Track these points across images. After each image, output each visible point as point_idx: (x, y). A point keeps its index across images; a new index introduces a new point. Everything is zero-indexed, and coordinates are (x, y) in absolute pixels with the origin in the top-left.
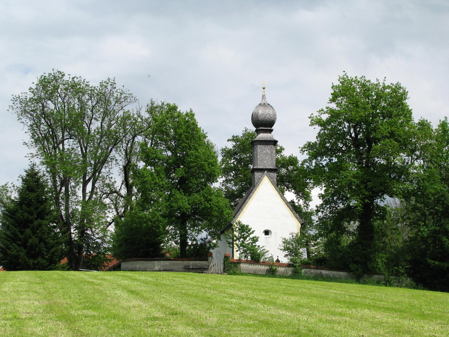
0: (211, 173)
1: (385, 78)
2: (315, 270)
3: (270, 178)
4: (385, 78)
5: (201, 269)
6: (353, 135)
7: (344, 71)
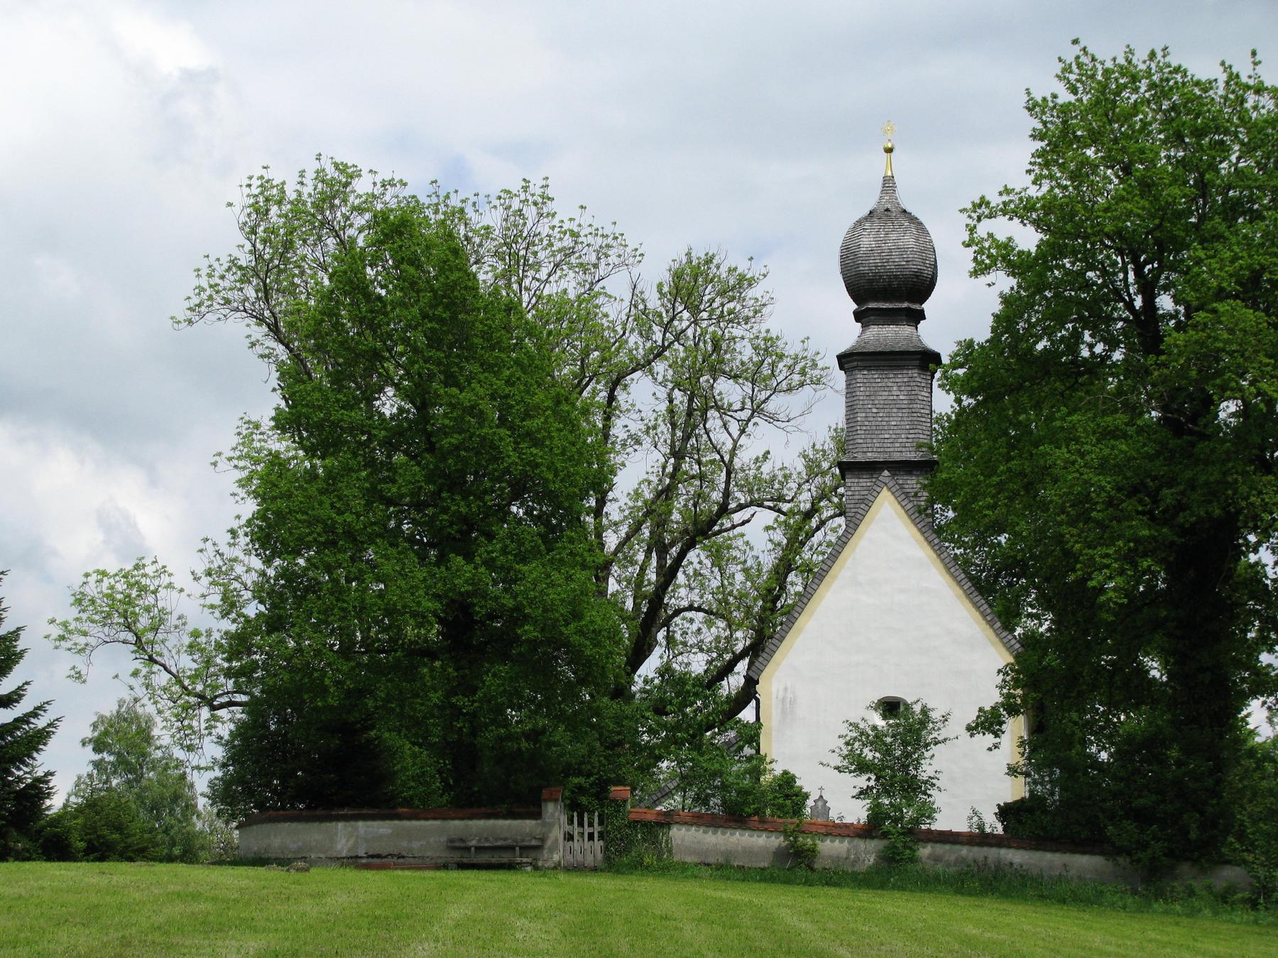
0: (524, 472)
1: (1254, 54)
2: (976, 849)
3: (903, 496)
4: (1254, 54)
5: (512, 848)
6: (1138, 303)
7: (1075, 42)
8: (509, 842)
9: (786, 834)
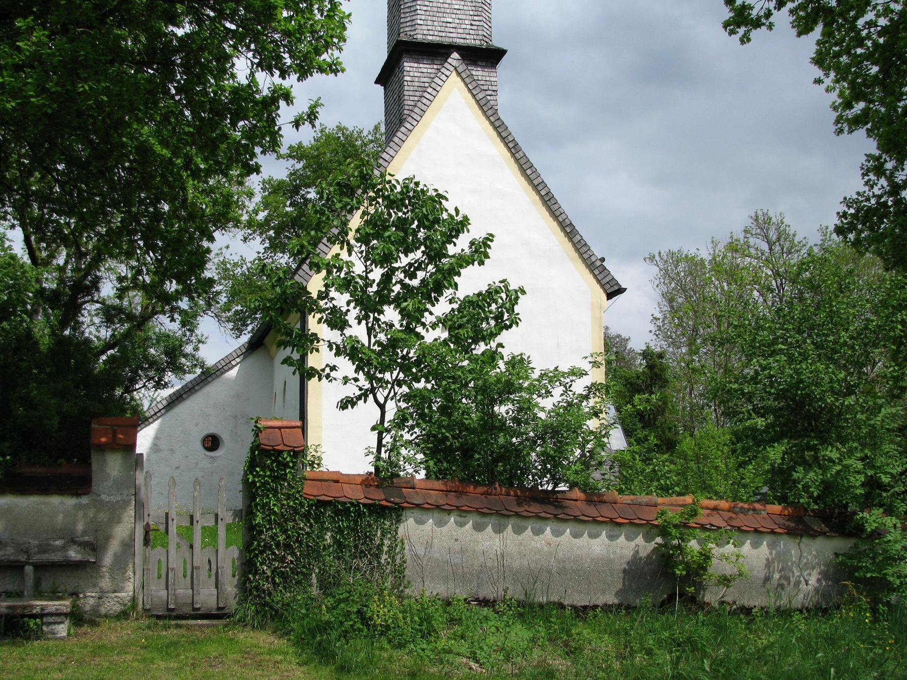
9: (651, 529)
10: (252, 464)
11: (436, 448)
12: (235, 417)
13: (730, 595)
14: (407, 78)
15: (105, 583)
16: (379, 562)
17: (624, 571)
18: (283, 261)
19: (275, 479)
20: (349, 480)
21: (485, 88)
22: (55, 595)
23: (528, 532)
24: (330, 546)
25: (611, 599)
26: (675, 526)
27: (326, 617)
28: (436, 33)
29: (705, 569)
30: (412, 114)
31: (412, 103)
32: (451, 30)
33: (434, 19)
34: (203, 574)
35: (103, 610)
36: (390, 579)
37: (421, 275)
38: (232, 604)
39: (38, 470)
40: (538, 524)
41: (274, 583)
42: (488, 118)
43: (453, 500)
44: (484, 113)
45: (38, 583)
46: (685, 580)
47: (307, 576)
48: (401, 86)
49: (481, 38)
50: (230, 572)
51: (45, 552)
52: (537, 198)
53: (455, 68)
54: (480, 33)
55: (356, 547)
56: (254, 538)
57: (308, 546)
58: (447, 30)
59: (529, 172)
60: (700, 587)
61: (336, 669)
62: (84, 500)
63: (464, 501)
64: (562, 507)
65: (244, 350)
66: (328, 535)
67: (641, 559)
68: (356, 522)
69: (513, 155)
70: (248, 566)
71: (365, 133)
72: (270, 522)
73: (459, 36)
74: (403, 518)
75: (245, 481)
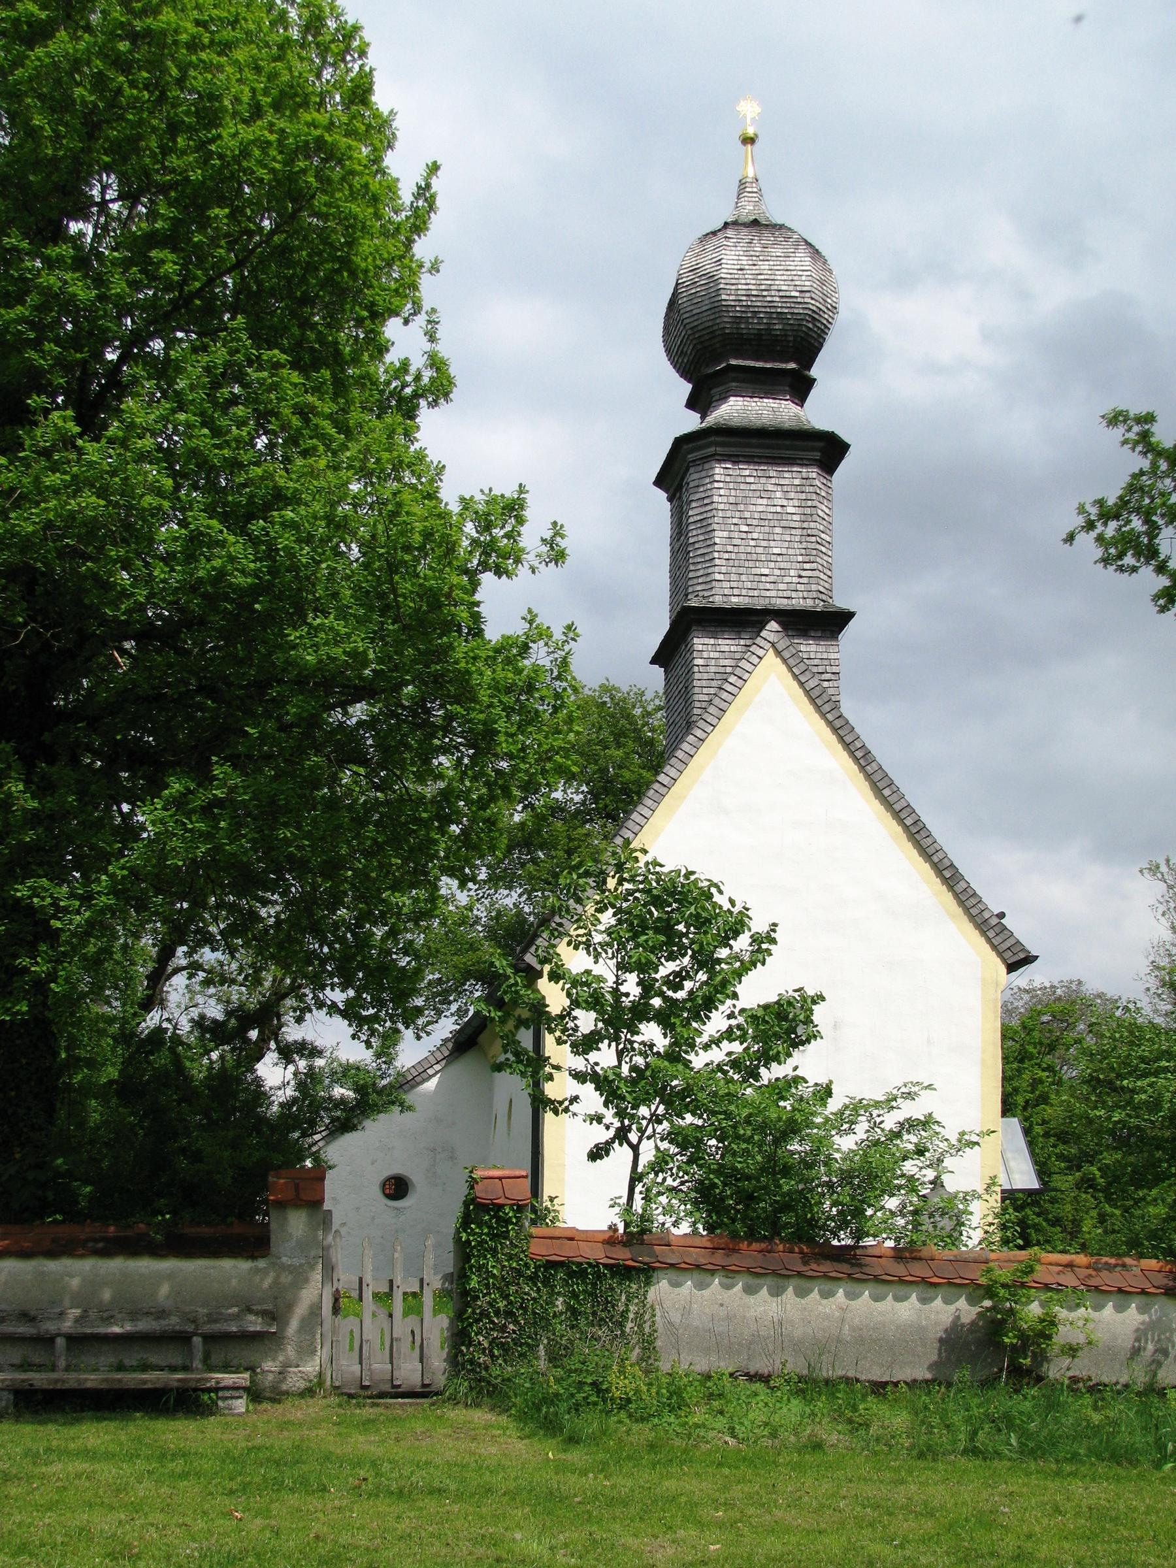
5: (181, 1339)
8: (173, 1322)
10: (466, 1221)
11: (705, 1198)
12: (434, 1150)
13: (1081, 1367)
14: (696, 662)
15: (290, 1351)
16: (623, 1332)
17: (941, 1340)
18: (509, 902)
19: (494, 1237)
20: (588, 1237)
21: (821, 669)
22: (226, 1368)
23: (815, 1295)
24: (561, 1313)
25: (922, 1373)
26: (1004, 1286)
27: (555, 1387)
28: (744, 592)
29: (1049, 1337)
30: (705, 716)
31: (706, 698)
32: (768, 586)
33: (741, 570)
34: (405, 1346)
35: (284, 1387)
36: (637, 1350)
37: (688, 985)
38: (440, 1380)
39: (204, 1230)
40: (828, 1286)
41: (492, 1356)
42: (823, 715)
43: (719, 1258)
44: (818, 708)
45: (206, 1359)
46: (1018, 1350)
47: (533, 1348)
48: (690, 672)
49: (815, 595)
50: (437, 1344)
51: (216, 1321)
52: (899, 829)
53: (773, 645)
54: (814, 587)
55: (594, 1314)
56: (468, 1305)
57: (534, 1313)
58: (761, 586)
59: (886, 792)
60: (1041, 1358)
61: (564, 1441)
62: (261, 1263)
63: (735, 1259)
64: (860, 1265)
65: (447, 1053)
66: (560, 1302)
67: (963, 1325)
68: (594, 1285)
69: (862, 769)
70: (460, 1337)
71: (649, 695)
72: (487, 1286)
73: (780, 594)
74: (654, 1280)
75: (457, 1240)
